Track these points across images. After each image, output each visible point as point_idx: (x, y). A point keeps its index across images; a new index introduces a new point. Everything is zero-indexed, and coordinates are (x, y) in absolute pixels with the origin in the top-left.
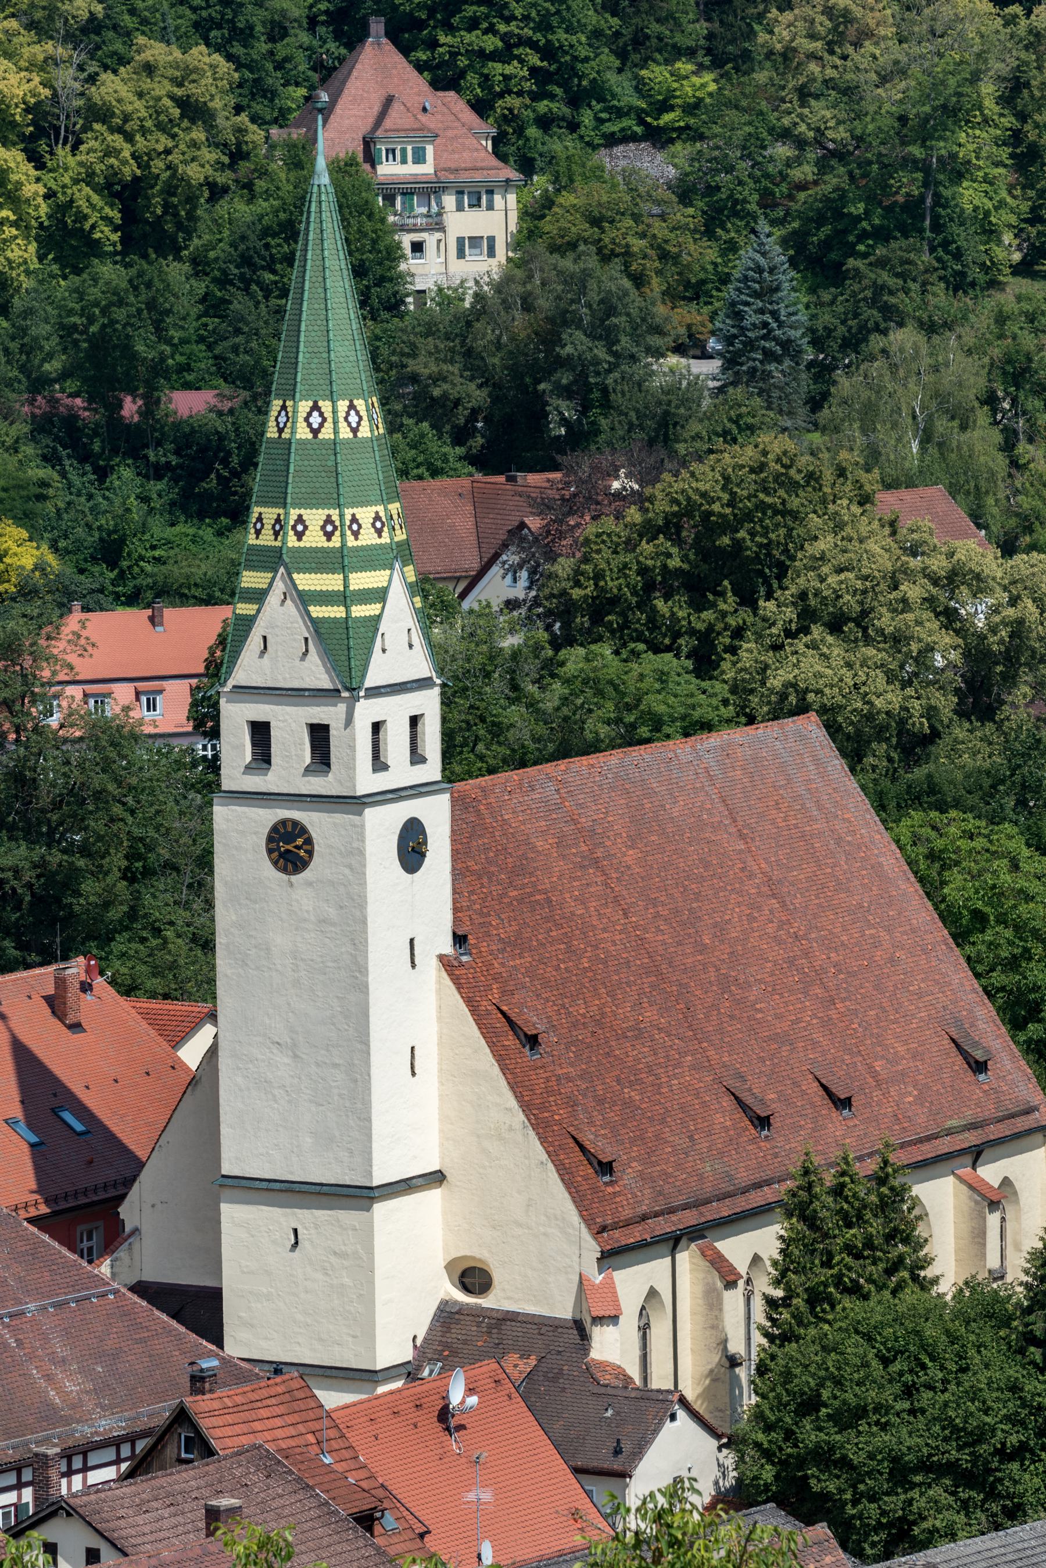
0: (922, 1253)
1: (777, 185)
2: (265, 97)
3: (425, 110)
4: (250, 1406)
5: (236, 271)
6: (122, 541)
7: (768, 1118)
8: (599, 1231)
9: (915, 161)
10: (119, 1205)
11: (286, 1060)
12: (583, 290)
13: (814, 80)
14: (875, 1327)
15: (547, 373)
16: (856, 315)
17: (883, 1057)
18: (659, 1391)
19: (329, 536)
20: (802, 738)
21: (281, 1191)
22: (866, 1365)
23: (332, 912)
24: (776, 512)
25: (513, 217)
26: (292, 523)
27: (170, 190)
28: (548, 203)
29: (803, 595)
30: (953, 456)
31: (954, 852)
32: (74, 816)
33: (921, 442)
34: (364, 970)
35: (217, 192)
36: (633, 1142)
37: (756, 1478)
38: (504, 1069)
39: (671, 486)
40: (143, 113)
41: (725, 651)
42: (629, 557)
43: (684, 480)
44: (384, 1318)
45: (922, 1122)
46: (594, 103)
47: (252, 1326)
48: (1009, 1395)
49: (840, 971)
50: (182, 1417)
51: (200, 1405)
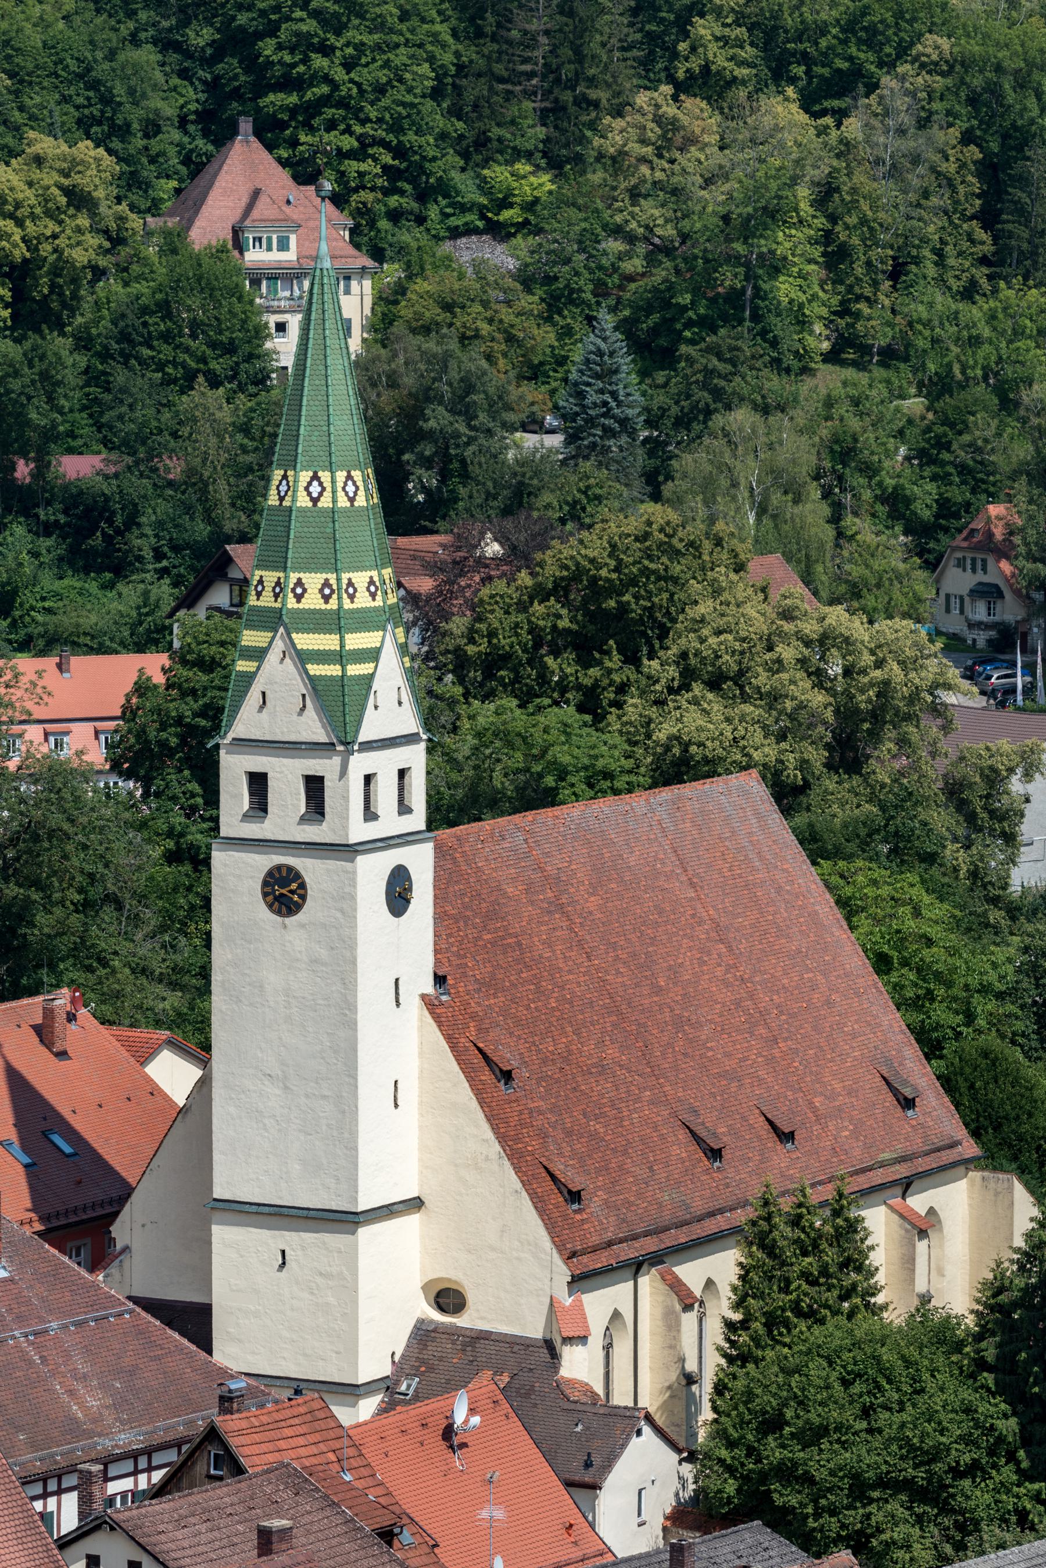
0: (872, 1281)
1: (610, 276)
2: (140, 188)
3: (288, 202)
4: (275, 1425)
5: (117, 346)
6: (15, 592)
7: (720, 1150)
8: (570, 1256)
9: (738, 257)
10: (111, 1223)
11: (278, 1092)
12: (445, 368)
13: (645, 181)
14: (835, 1351)
15: (410, 446)
16: (688, 397)
17: (822, 1094)
18: (616, 1407)
19: (326, 599)
20: (745, 793)
21: (270, 1214)
22: (828, 1387)
23: (323, 953)
24: (659, 578)
25: (368, 302)
26: (291, 586)
27: (56, 272)
28: (400, 290)
29: (684, 655)
30: (786, 527)
31: (861, 899)
32: (29, 852)
33: (757, 514)
34: (353, 1007)
35: (99, 273)
36: (598, 1171)
37: (720, 1491)
38: (482, 1102)
39: (560, 552)
40: (33, 201)
41: (611, 705)
42: (521, 617)
43: (571, 547)
44: (366, 1335)
45: (858, 1156)
46: (440, 198)
47: (240, 1341)
48: (964, 1416)
49: (782, 1013)
50: (212, 1435)
51: (230, 1425)
